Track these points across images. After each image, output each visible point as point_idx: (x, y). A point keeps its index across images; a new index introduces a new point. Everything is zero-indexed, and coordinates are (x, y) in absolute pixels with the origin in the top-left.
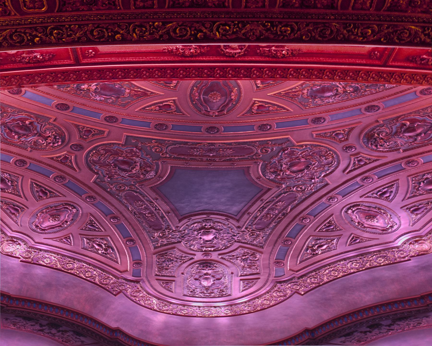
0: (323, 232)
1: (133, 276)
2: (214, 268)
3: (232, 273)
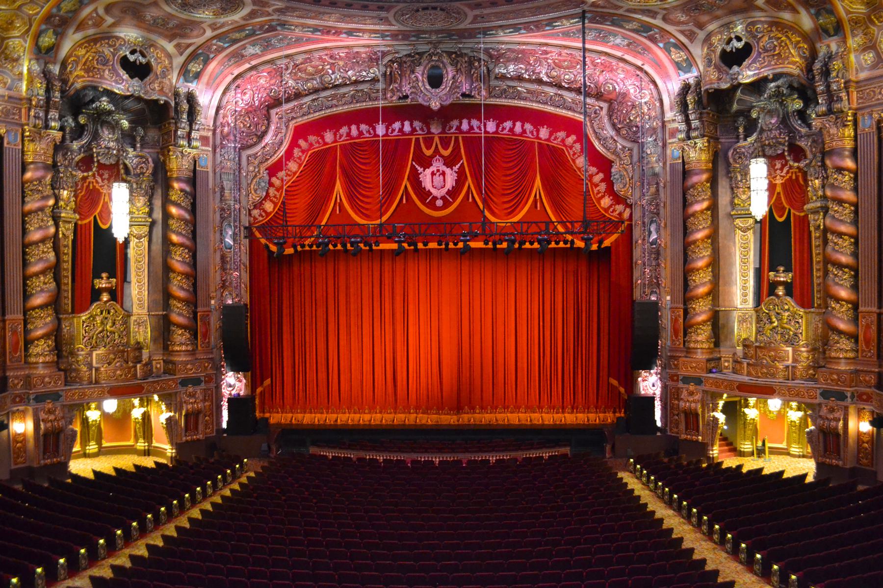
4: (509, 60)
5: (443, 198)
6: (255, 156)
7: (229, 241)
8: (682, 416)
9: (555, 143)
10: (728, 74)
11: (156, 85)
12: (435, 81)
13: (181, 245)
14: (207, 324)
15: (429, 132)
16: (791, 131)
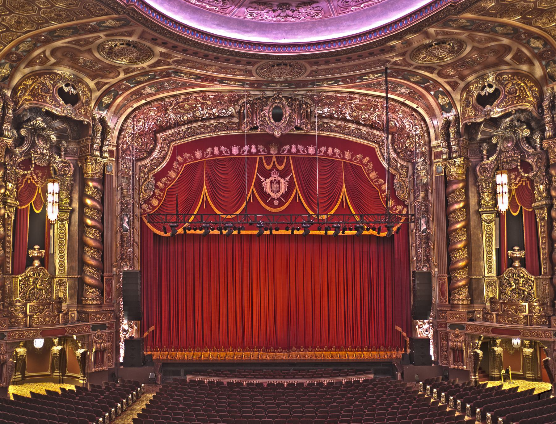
4: (325, 104)
5: (279, 199)
6: (145, 166)
7: (126, 225)
8: (451, 352)
9: (355, 163)
10: (482, 111)
11: (82, 110)
12: (278, 117)
13: (93, 227)
14: (110, 285)
15: (269, 153)
16: (522, 152)
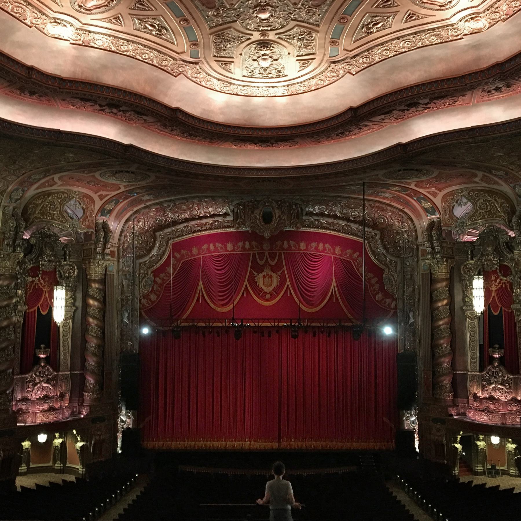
0: (380, 8)
1: (191, 57)
2: (272, 48)
3: (289, 54)
7: (126, 320)
15: (262, 249)
